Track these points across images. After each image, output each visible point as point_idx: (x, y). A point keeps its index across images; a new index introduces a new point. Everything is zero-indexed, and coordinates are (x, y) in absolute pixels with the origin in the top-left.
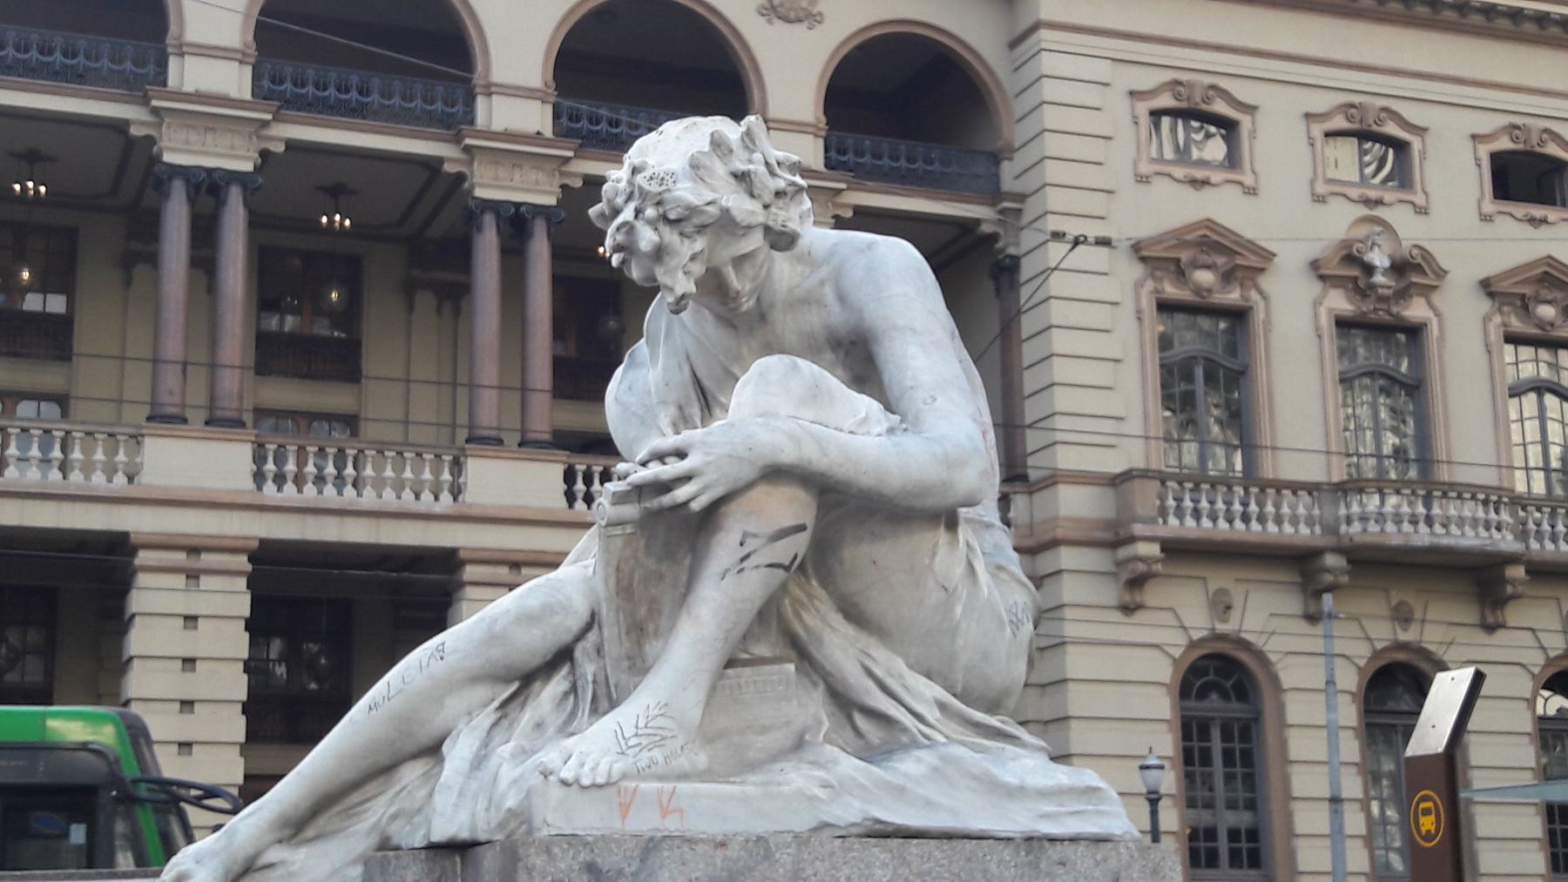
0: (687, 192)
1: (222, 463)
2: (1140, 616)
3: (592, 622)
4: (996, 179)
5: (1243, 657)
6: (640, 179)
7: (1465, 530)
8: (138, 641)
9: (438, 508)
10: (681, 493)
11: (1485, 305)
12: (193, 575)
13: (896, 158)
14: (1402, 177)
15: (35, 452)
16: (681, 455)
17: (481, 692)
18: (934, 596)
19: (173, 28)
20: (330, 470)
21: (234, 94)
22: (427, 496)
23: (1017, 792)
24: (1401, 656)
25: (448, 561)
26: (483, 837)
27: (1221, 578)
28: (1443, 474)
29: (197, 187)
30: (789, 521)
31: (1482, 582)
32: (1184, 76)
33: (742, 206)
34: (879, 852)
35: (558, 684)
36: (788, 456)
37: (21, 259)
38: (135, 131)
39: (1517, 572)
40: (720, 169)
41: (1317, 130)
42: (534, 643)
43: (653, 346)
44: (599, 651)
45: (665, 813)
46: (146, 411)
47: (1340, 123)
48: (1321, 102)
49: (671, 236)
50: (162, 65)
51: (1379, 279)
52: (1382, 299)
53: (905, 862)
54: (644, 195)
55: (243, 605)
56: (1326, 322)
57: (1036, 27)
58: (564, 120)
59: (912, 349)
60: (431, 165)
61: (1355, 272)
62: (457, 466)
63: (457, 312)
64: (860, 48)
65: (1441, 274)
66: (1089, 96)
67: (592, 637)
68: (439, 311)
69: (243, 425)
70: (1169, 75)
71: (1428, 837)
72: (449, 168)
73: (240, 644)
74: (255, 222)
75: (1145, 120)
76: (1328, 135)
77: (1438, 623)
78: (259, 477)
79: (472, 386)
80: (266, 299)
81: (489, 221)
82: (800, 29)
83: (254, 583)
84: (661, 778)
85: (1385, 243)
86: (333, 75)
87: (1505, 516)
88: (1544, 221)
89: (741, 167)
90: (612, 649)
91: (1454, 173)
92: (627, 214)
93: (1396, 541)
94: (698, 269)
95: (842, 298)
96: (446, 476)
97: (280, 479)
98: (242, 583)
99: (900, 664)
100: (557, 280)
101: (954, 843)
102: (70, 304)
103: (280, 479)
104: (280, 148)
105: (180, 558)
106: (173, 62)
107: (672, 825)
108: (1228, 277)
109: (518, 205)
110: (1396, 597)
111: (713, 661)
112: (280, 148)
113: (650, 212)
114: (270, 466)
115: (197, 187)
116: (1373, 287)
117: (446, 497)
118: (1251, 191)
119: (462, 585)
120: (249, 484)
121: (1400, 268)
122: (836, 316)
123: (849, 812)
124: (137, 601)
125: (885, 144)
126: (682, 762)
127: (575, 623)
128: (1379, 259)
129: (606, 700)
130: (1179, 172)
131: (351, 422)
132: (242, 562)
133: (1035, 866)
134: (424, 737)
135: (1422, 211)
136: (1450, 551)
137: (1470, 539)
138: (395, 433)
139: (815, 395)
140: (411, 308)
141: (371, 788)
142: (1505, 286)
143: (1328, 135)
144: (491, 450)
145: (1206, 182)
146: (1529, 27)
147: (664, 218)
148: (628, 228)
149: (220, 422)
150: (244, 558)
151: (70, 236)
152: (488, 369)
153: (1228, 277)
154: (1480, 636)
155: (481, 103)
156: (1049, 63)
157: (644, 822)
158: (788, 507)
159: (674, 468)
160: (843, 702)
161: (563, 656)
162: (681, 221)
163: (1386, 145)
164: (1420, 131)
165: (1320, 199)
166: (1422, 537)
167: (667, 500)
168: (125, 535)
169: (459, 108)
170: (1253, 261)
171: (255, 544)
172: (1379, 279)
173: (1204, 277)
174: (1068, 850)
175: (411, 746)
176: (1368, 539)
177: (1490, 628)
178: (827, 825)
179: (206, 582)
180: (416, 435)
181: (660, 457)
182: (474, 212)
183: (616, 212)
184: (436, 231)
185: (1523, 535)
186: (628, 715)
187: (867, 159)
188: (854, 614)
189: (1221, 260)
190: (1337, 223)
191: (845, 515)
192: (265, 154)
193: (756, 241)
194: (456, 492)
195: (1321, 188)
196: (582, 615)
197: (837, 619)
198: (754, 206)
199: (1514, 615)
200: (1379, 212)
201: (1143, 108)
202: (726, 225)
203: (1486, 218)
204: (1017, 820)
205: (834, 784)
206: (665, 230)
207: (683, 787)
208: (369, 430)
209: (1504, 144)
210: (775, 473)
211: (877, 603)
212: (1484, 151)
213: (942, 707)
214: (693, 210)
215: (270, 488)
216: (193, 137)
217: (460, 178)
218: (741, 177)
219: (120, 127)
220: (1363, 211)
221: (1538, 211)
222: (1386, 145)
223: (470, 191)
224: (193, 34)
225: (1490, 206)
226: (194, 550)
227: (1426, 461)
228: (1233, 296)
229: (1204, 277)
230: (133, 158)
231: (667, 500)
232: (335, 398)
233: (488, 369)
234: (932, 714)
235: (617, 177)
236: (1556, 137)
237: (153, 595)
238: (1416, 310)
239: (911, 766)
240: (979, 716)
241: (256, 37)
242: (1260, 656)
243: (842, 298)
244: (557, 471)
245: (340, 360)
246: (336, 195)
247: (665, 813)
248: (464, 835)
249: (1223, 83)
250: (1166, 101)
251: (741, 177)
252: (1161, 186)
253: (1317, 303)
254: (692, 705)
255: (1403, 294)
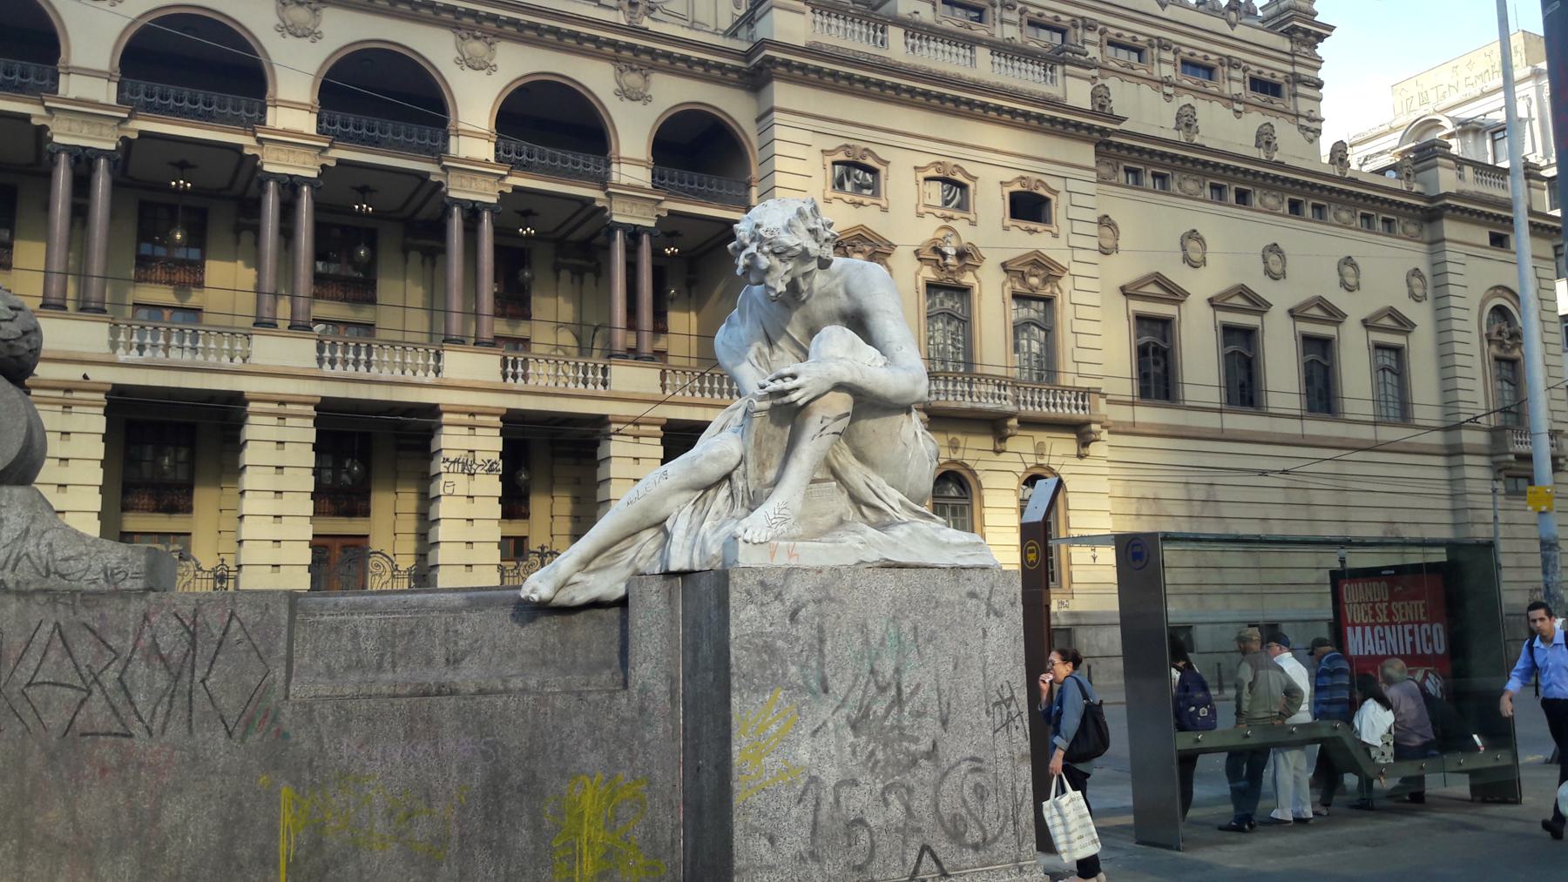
0: (787, 240)
1: (299, 352)
2: (1003, 455)
3: (743, 460)
4: (445, 149)
5: (965, 473)
6: (761, 231)
7: (986, 400)
8: (249, 456)
9: (427, 381)
10: (794, 396)
11: (1004, 276)
12: (282, 417)
13: (691, 183)
14: (963, 206)
15: (187, 343)
16: (794, 377)
17: (685, 496)
18: (901, 447)
19: (270, 90)
20: (351, 356)
21: (306, 131)
22: (420, 373)
23: (946, 545)
24: (952, 467)
25: (433, 411)
26: (697, 568)
27: (1041, 436)
28: (978, 369)
29: (284, 186)
30: (843, 411)
31: (994, 426)
32: (1025, 174)
33: (813, 247)
34: (888, 575)
35: (724, 492)
36: (847, 378)
37: (172, 225)
38: (247, 151)
39: (1014, 422)
40: (803, 228)
41: (921, 176)
42: (713, 471)
43: (741, 313)
44: (745, 475)
45: (791, 556)
46: (40, 301)
47: (932, 173)
48: (924, 160)
49: (775, 261)
50: (263, 112)
51: (949, 261)
52: (951, 272)
53: (900, 580)
54: (762, 239)
55: (312, 436)
56: (922, 285)
57: (771, 110)
58: (127, 94)
59: (889, 322)
60: (586, 202)
61: (938, 257)
62: (438, 356)
63: (434, 265)
64: (671, 118)
65: (982, 259)
66: (799, 151)
67: (741, 468)
68: (423, 262)
69: (104, 311)
70: (844, 142)
71: (1032, 564)
72: (433, 178)
73: (310, 459)
74: (318, 207)
75: (829, 166)
76: (927, 179)
77: (974, 450)
78: (320, 360)
79: (447, 311)
80: (320, 254)
81: (618, 233)
82: (639, 104)
83: (317, 423)
84: (785, 539)
85: (953, 240)
86: (338, 117)
87: (1009, 392)
88: (861, 204)
89: (813, 226)
90: (751, 475)
91: (991, 200)
92: (753, 248)
93: (954, 405)
94: (788, 279)
95: (848, 293)
96: (432, 362)
97: (332, 362)
98: (310, 422)
99: (883, 483)
100: (498, 250)
101: (904, 572)
102: (315, 267)
103: (332, 362)
104: (333, 164)
105: (465, 418)
106: (270, 111)
107: (793, 562)
108: (1045, 281)
109: (474, 202)
110: (951, 437)
111: (806, 482)
112: (333, 164)
113: (766, 249)
114: (327, 354)
115: (284, 186)
116: (946, 265)
117: (431, 374)
118: (885, 210)
119: (440, 426)
120: (107, 349)
121: (961, 255)
122: (844, 303)
123: (873, 556)
124: (249, 432)
125: (686, 175)
126: (794, 531)
127: (734, 462)
128: (950, 251)
129: (754, 502)
130: (847, 198)
131: (369, 328)
132: (310, 410)
133: (957, 581)
134: (656, 517)
135: (973, 224)
136: (980, 411)
137: (990, 405)
138: (397, 336)
139: (852, 347)
140: (406, 261)
141: (623, 544)
142: (1013, 266)
143: (927, 179)
144: (458, 347)
145: (861, 204)
146: (1034, 122)
147: (772, 251)
148: (752, 256)
149: (299, 327)
150: (102, 396)
151: (203, 213)
152: (456, 302)
153: (1045, 281)
154: (993, 456)
155: (453, 140)
156: (778, 132)
157: (782, 561)
158: (843, 402)
159: (789, 384)
160: (856, 500)
161: (728, 477)
162: (782, 253)
163: (956, 189)
164: (974, 178)
165: (920, 215)
166: (967, 403)
167: (786, 399)
168: (241, 393)
169: (439, 143)
170: (885, 249)
171: (109, 388)
172: (949, 261)
173: (1034, 281)
174: (971, 573)
175: (647, 523)
176: (939, 404)
177: (997, 452)
178: (862, 562)
179: (289, 421)
180: (409, 337)
181: (782, 377)
182: (612, 228)
183: (744, 247)
184: (423, 215)
185: (1017, 402)
186: (768, 509)
187: (676, 183)
188: (860, 456)
189: (867, 248)
190: (927, 230)
191: (868, 403)
192: (323, 167)
193: (814, 265)
194: (438, 371)
195: (922, 210)
196: (738, 458)
197: (853, 460)
198: (816, 246)
199: (1011, 444)
200: (951, 223)
201: (829, 160)
202: (804, 256)
203: (1006, 229)
204: (947, 559)
205: (861, 544)
206: (772, 257)
207: (799, 544)
208: (536, 349)
209: (1017, 187)
210: (839, 387)
211: (874, 452)
212: (1007, 191)
213: (902, 503)
214: (790, 248)
215: (510, 380)
216: (465, 182)
217: (440, 184)
218: (812, 231)
219: (238, 148)
220: (942, 223)
221: (1033, 225)
222: (956, 189)
223: (445, 194)
224: (623, 154)
225: (1008, 222)
226: (282, 403)
227: (969, 363)
228: (1047, 291)
229: (1034, 281)
230: (245, 166)
231: (786, 399)
232: (365, 315)
233: (456, 302)
234: (898, 507)
235: (743, 229)
236: (961, 170)
237: (257, 429)
238: (967, 279)
239: (899, 532)
240: (918, 508)
241: (121, 65)
242: (973, 472)
243: (848, 293)
244: (498, 359)
245: (362, 290)
246: (364, 192)
247: (791, 556)
248: (686, 567)
249: (1044, 179)
250: (841, 157)
251: (812, 231)
252: (1015, 232)
253: (917, 274)
254: (797, 504)
255: (962, 270)
